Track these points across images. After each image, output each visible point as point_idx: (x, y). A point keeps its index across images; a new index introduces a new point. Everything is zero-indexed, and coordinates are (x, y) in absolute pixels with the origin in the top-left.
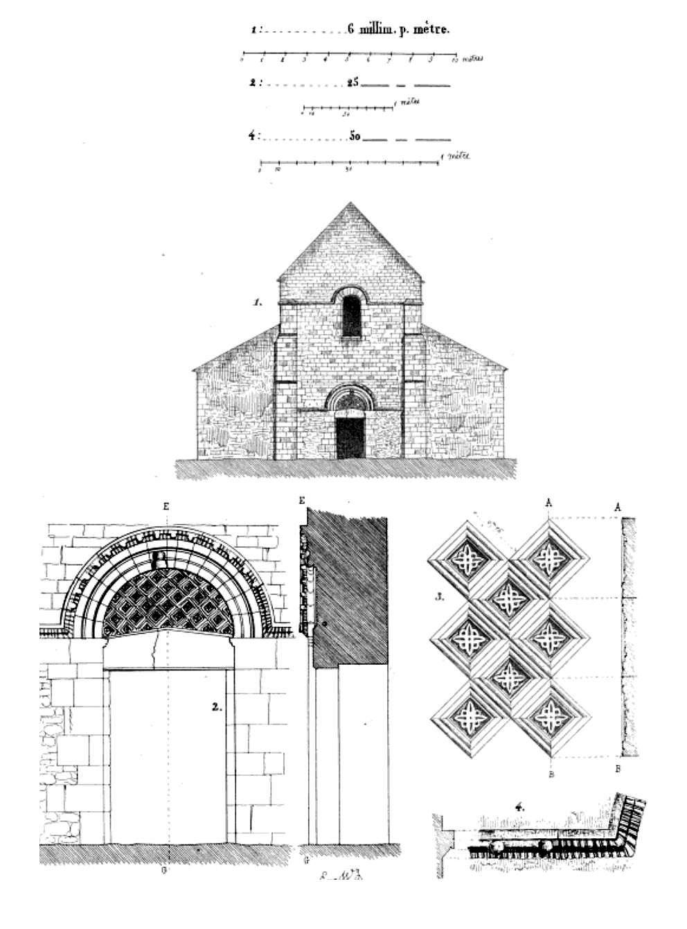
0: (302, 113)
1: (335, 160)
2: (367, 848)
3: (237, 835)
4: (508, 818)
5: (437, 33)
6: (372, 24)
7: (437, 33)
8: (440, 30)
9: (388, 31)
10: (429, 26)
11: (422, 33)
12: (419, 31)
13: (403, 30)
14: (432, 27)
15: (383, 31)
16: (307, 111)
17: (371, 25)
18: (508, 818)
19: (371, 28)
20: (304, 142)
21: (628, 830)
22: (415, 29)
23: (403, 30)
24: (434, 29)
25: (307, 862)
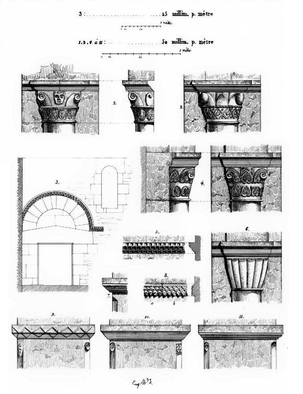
0: (121, 29)
1: (146, 25)
2: (193, 291)
3: (74, 255)
4: (217, 132)
5: (209, 15)
6: (178, 39)
7: (209, 15)
8: (210, 15)
9: (184, 15)
10: (206, 41)
11: (203, 44)
12: (200, 15)
13: (193, 15)
14: (207, 41)
15: (181, 15)
16: (123, 28)
17: (177, 40)
18: (217, 132)
19: (177, 13)
20: (121, 30)
21: (222, 251)
22: (200, 41)
23: (193, 15)
24: (208, 14)
25: (166, 275)
